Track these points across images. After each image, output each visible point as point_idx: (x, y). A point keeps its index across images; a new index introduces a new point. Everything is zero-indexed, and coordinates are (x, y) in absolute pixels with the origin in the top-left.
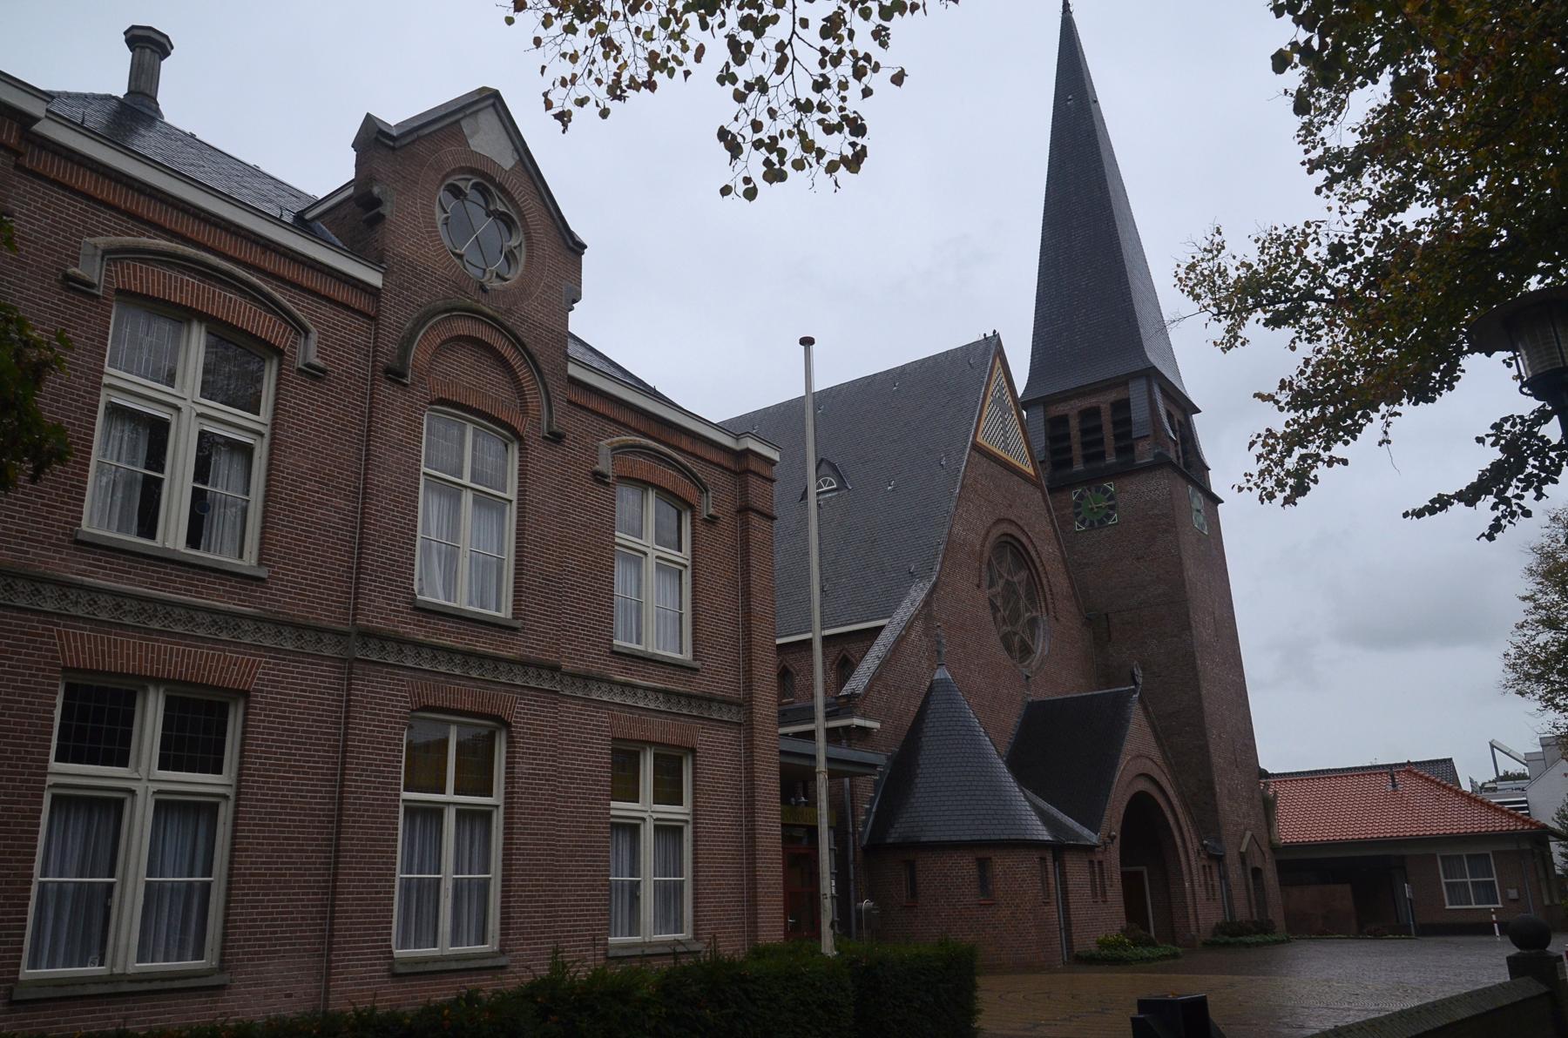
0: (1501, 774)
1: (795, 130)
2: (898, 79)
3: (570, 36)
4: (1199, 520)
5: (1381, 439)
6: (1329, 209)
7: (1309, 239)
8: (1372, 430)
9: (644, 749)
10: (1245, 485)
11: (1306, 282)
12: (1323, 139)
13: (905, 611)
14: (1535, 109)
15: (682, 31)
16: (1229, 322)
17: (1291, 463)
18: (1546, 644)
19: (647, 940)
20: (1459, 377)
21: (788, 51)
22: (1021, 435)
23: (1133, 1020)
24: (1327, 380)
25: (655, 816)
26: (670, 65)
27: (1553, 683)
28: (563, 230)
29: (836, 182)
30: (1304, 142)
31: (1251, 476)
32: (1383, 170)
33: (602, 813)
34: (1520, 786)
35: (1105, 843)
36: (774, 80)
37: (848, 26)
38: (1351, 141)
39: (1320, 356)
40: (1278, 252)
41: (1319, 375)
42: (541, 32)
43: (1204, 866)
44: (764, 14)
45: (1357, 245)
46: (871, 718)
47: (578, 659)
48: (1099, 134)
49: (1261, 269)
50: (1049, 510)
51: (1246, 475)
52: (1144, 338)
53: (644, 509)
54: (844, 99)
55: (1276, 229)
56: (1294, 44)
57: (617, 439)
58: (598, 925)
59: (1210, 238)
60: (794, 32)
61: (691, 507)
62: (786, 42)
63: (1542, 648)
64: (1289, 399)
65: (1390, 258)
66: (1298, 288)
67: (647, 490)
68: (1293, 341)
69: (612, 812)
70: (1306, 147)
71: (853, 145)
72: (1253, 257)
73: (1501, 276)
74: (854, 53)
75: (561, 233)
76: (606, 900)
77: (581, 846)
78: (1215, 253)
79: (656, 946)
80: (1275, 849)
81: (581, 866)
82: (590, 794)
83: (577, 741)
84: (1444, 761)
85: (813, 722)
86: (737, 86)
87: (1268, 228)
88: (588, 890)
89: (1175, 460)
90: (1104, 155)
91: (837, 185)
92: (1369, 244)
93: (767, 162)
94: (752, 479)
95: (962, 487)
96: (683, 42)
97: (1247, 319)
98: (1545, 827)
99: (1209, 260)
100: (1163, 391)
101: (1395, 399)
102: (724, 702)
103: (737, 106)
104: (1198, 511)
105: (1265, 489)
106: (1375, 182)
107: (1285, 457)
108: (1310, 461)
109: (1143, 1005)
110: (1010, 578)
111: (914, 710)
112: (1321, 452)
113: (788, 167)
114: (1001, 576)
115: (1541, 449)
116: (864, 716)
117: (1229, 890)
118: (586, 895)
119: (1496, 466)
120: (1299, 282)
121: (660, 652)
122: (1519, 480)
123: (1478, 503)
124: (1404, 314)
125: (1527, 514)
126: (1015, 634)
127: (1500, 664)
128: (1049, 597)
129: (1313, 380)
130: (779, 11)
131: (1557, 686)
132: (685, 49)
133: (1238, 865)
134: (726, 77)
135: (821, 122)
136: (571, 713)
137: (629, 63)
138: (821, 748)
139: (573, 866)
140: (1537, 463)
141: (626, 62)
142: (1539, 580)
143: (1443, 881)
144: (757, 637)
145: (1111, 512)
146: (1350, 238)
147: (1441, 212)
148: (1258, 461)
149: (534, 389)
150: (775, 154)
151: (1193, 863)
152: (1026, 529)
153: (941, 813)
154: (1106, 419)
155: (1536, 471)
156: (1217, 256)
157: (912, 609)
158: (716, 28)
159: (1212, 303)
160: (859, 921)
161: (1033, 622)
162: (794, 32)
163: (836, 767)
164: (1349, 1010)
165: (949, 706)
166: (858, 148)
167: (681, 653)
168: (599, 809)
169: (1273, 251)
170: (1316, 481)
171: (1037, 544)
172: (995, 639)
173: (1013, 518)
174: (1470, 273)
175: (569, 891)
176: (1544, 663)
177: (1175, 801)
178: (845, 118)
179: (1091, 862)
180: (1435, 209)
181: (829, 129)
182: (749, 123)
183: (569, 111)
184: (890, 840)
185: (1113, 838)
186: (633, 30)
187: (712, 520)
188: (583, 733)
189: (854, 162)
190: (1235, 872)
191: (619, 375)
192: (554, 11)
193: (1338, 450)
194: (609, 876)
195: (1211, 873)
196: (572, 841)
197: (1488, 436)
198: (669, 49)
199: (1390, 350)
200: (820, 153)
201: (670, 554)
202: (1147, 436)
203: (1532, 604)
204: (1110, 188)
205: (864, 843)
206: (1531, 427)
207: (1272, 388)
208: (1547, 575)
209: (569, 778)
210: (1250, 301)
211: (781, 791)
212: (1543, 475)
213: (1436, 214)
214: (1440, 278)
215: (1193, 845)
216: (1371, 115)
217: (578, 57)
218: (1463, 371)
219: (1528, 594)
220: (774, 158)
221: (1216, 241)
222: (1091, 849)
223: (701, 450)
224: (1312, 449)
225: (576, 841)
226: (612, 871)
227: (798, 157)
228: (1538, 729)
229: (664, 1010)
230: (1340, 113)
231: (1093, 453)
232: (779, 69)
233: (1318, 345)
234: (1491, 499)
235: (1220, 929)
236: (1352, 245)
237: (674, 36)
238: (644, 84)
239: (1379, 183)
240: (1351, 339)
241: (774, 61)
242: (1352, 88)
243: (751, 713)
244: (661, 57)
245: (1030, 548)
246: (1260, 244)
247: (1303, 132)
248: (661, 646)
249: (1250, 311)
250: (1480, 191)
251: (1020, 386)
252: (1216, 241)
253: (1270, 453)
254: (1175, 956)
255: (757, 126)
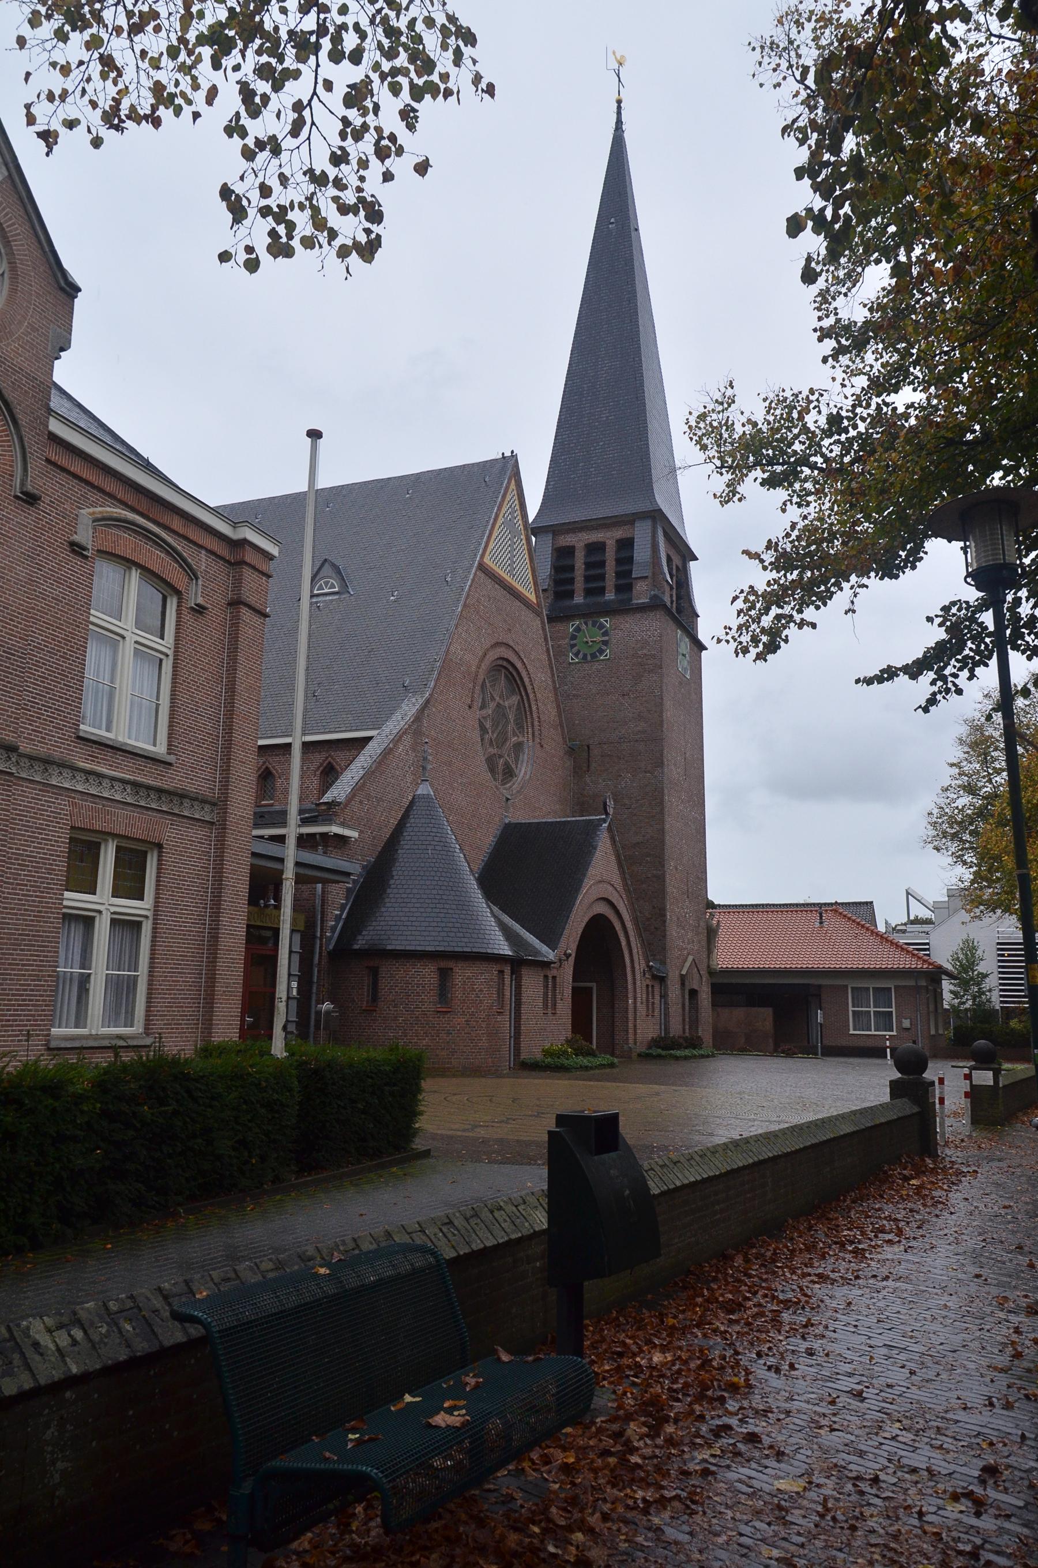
0: (912, 918)
1: (307, 203)
2: (422, 168)
3: (61, 44)
4: (683, 664)
5: (847, 608)
6: (834, 379)
7: (812, 406)
8: (841, 598)
9: (106, 841)
10: (723, 637)
11: (803, 448)
12: (836, 309)
13: (395, 724)
14: (1018, 315)
15: (194, 66)
16: (730, 476)
17: (766, 621)
18: (964, 807)
19: (94, 1032)
20: (922, 558)
21: (306, 113)
22: (527, 561)
23: (549, 1132)
24: (809, 545)
25: (113, 909)
26: (177, 101)
27: (964, 842)
28: (55, 267)
29: (347, 269)
30: (819, 309)
31: (730, 629)
32: (885, 349)
33: (55, 903)
34: (926, 930)
35: (560, 960)
36: (288, 143)
37: (375, 99)
38: (860, 315)
39: (806, 522)
40: (782, 414)
41: (803, 539)
42: (26, 31)
43: (647, 986)
44: (285, 65)
45: (853, 419)
46: (349, 827)
47: (39, 742)
48: (636, 264)
49: (765, 428)
50: (546, 639)
51: (725, 628)
52: (654, 479)
53: (126, 587)
54: (362, 179)
55: (784, 391)
56: (809, 210)
57: (100, 509)
58: (41, 1015)
59: (723, 390)
60: (315, 93)
61: (178, 593)
62: (305, 103)
63: (960, 810)
64: (773, 560)
65: (879, 436)
66: (795, 452)
67: (130, 569)
68: (785, 504)
69: (65, 903)
70: (820, 314)
71: (368, 231)
72: (759, 416)
73: (971, 468)
74: (379, 130)
75: (51, 268)
76: (51, 991)
77: (28, 935)
78: (726, 405)
79: (103, 1038)
80: (712, 973)
81: (26, 955)
82: (43, 883)
83: (31, 827)
84: (867, 903)
85: (285, 827)
86: (246, 141)
87: (776, 389)
88: (32, 980)
89: (668, 604)
90: (639, 288)
91: (348, 272)
92: (863, 419)
93: (273, 234)
94: (247, 572)
95: (465, 606)
96: (194, 79)
97: (747, 475)
98: (940, 967)
99: (719, 412)
100: (666, 534)
101: (864, 573)
102: (196, 799)
103: (243, 164)
104: (684, 655)
105: (741, 643)
106: (877, 360)
107: (762, 615)
108: (783, 621)
109: (561, 1119)
110: (501, 702)
111: (394, 822)
112: (795, 613)
113: (296, 243)
114: (493, 699)
115: (979, 634)
116: (343, 825)
117: (667, 1009)
118: (29, 985)
119: (940, 645)
120: (797, 447)
121: (129, 742)
122: (957, 661)
123: (920, 678)
124: (883, 492)
125: (959, 692)
126: (500, 756)
127: (924, 822)
128: (536, 723)
129: (796, 543)
130: (301, 66)
131: (967, 845)
132: (196, 87)
133: (678, 986)
134: (236, 129)
135: (336, 199)
136: (27, 797)
137: (131, 89)
138: (290, 852)
139: (18, 955)
140: (974, 647)
141: (127, 88)
142: (966, 749)
143: (851, 1009)
144: (237, 736)
145: (604, 647)
146: (847, 411)
147: (928, 399)
148: (739, 615)
149: (9, 441)
150: (283, 225)
151: (638, 983)
152: (523, 656)
153: (409, 923)
154: (610, 556)
155: (972, 654)
156: (727, 409)
157: (402, 723)
158: (229, 71)
159: (717, 455)
160: (318, 1022)
161: (518, 747)
162: (315, 93)
163: (302, 871)
164: (754, 1120)
165: (428, 821)
166: (373, 236)
167: (155, 745)
168: (51, 898)
169: (778, 412)
170: (786, 641)
171: (531, 671)
172: (481, 760)
173: (511, 643)
174: (944, 461)
175: (11, 979)
176: (959, 823)
177: (629, 925)
178: (361, 200)
179: (546, 977)
180: (923, 396)
181: (344, 209)
182: (257, 185)
183: (56, 131)
184: (356, 947)
185: (568, 956)
186: (138, 53)
187: (199, 610)
188: (39, 819)
189: (369, 250)
190: (674, 991)
191: (108, 439)
192: (43, 10)
193: (810, 614)
194: (57, 967)
195: (653, 992)
196: (18, 930)
197: (937, 616)
198: (177, 84)
199: (867, 524)
200: (333, 234)
201: (153, 640)
202: (646, 577)
203: (957, 771)
204: (640, 322)
205: (331, 947)
206: (974, 613)
207: (759, 547)
208: (974, 745)
209: (19, 864)
210: (751, 459)
211: (250, 893)
212: (977, 658)
213: (924, 400)
214: (917, 462)
215: (640, 965)
216: (881, 294)
217: (71, 71)
218: (926, 553)
219: (955, 761)
220: (281, 230)
221: (727, 394)
222: (546, 965)
223: (193, 533)
224: (787, 610)
225: (23, 930)
226: (61, 960)
227: (308, 234)
228: (946, 882)
229: (99, 1105)
230: (854, 286)
231: (594, 591)
232: (295, 130)
233: (805, 511)
234: (931, 675)
235: (655, 1043)
236: (848, 418)
237: (185, 69)
238: (146, 117)
239: (880, 361)
240: (836, 509)
241: (290, 121)
242: (869, 263)
243: (226, 813)
244: (168, 90)
245: (524, 674)
246: (767, 404)
247: (819, 299)
248: (134, 737)
249: (750, 468)
250: (964, 384)
251: (533, 507)
252: (727, 394)
253: (750, 609)
254: (612, 1065)
255: (265, 191)
